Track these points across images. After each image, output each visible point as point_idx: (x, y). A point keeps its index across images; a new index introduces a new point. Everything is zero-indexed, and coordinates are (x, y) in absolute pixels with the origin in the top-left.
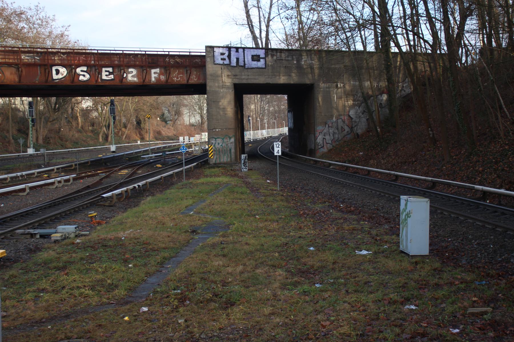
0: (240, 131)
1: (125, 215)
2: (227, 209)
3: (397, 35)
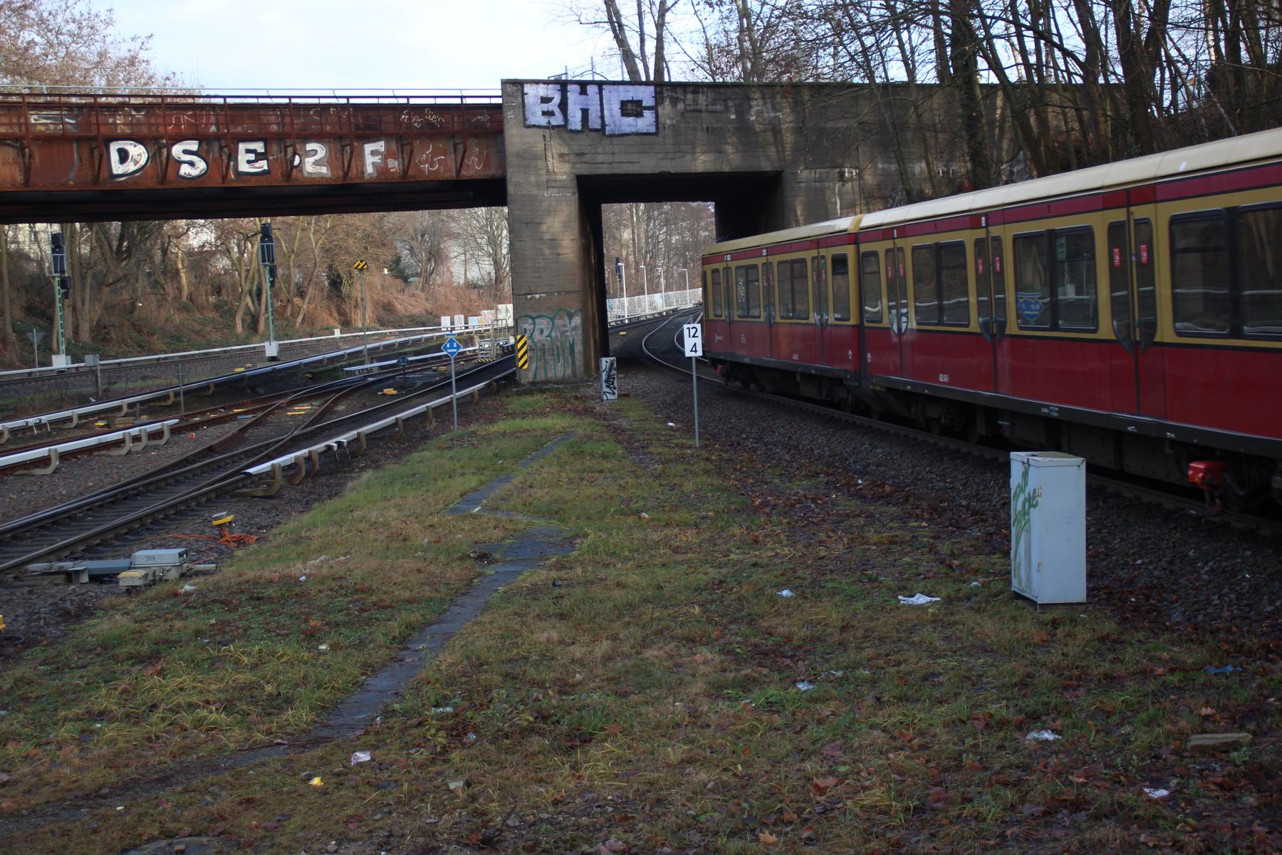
0: (595, 298)
1: (306, 518)
2: (568, 497)
3: (995, 40)
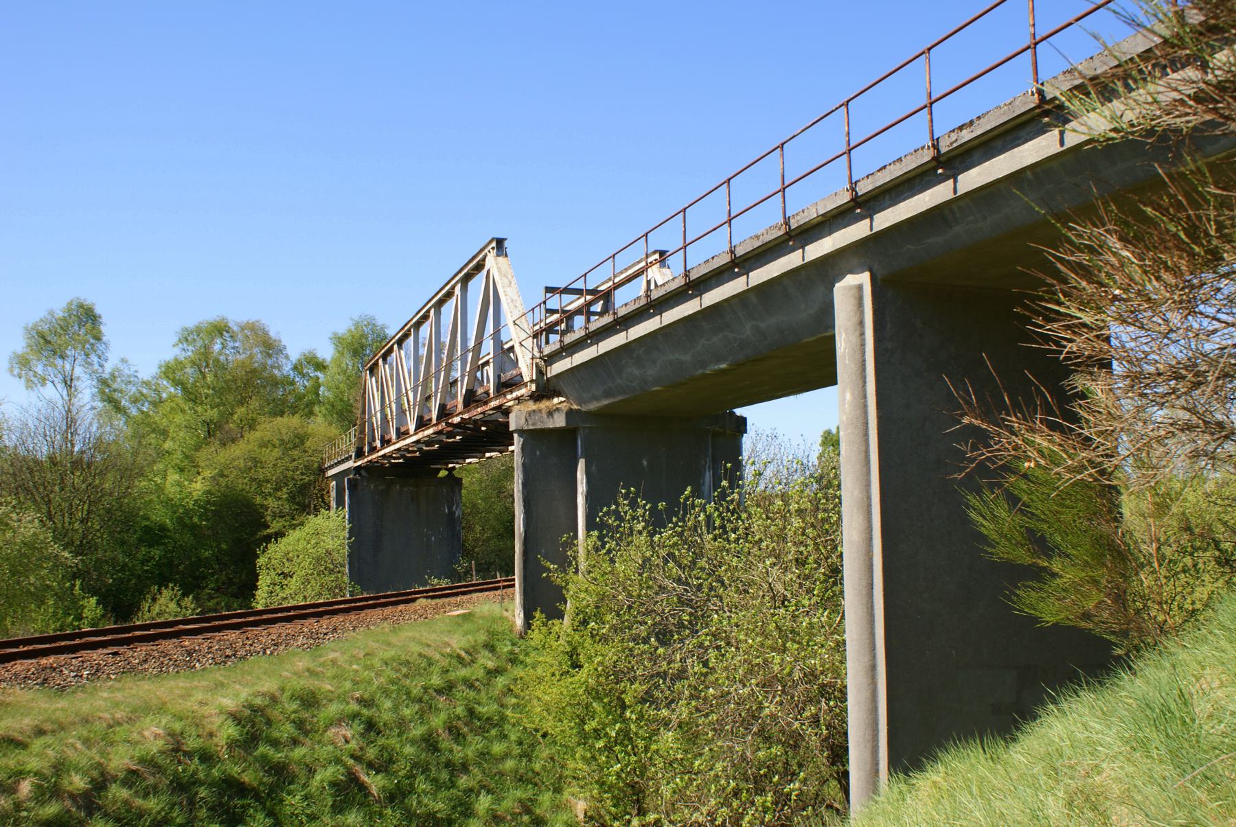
3: (952, 180)
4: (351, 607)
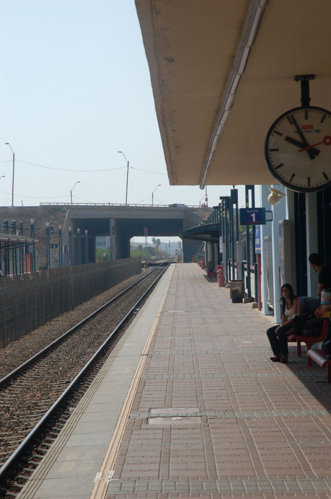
0: (124, 205)
4: (110, 218)
